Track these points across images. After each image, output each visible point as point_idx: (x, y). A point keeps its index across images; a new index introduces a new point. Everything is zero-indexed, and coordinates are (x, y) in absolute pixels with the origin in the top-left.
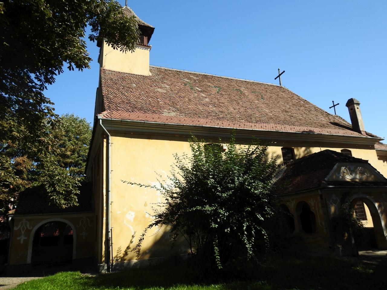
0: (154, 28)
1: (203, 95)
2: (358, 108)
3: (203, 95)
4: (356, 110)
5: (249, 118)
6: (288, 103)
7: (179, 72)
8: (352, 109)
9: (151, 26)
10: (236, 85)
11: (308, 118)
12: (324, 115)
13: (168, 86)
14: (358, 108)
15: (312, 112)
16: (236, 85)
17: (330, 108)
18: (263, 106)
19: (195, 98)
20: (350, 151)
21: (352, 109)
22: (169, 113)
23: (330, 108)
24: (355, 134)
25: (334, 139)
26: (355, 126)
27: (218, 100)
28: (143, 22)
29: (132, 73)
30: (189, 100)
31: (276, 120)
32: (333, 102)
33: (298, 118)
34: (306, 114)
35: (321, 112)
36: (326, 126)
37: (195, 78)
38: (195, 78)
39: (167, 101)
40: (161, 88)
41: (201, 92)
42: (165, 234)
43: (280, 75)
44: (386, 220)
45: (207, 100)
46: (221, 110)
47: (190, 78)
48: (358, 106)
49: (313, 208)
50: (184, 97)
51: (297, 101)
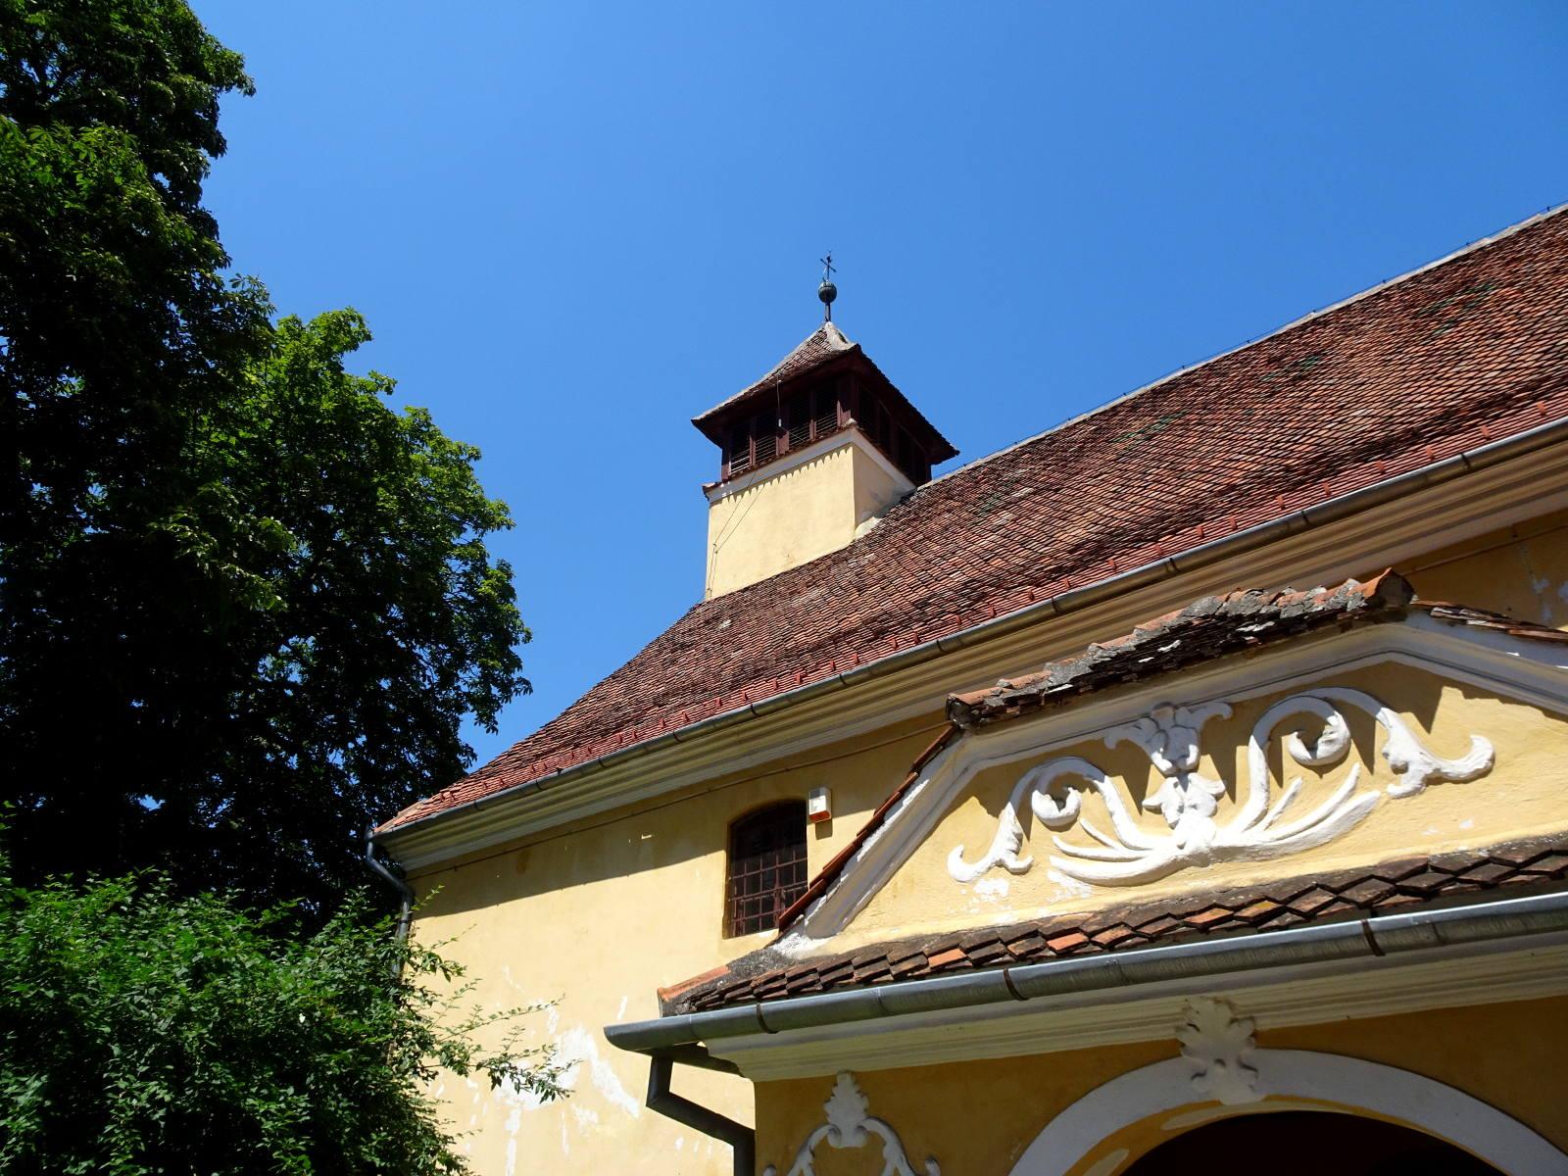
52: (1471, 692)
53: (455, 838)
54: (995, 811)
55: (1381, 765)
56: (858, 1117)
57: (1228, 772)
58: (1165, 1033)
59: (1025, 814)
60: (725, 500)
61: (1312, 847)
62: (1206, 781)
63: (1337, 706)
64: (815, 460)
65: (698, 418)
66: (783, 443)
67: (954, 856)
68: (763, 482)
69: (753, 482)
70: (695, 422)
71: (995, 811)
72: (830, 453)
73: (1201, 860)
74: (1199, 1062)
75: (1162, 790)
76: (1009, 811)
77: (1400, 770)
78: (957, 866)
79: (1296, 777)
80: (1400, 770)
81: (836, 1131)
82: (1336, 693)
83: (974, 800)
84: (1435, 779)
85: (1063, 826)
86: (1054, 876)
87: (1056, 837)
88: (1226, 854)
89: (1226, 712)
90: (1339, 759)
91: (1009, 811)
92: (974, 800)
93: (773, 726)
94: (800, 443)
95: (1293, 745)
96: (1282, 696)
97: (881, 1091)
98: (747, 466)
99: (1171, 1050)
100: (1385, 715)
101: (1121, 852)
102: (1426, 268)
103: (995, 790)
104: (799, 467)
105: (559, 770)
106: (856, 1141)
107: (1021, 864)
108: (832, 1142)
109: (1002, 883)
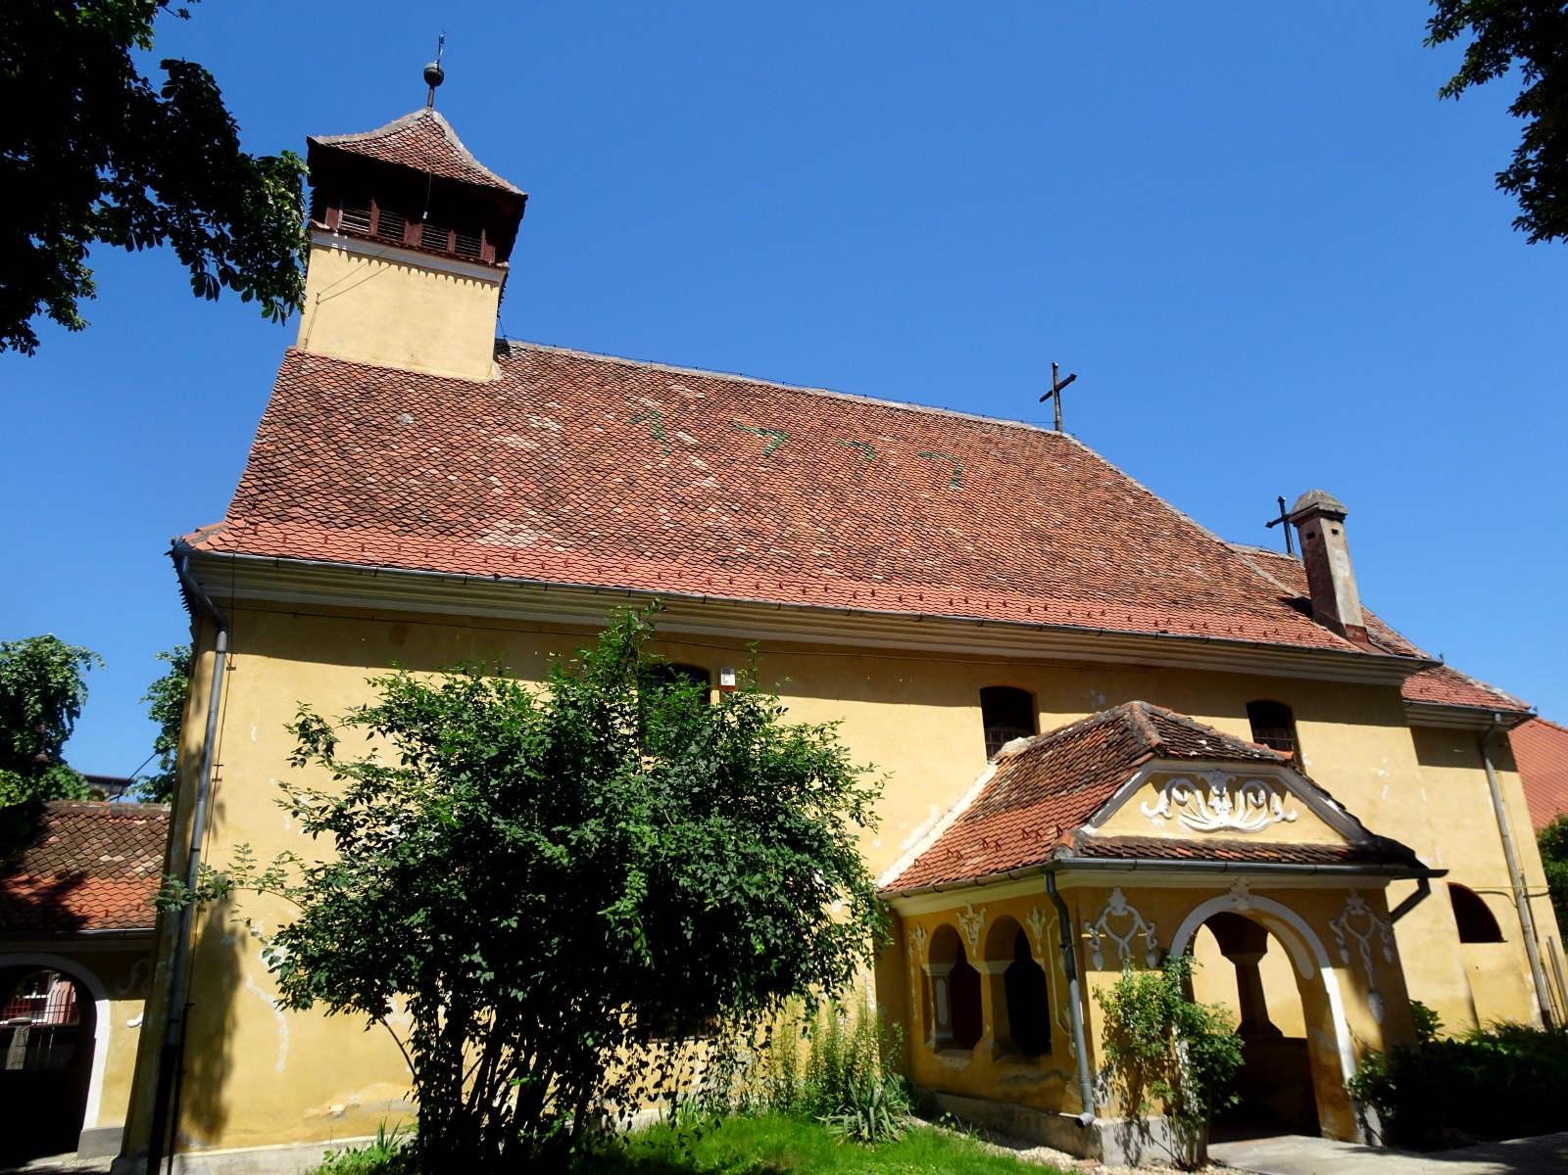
0: (525, 197)
1: (698, 463)
2: (1335, 532)
3: (698, 463)
4: (1328, 537)
5: (859, 563)
6: (1060, 504)
7: (631, 368)
8: (1311, 536)
9: (516, 190)
10: (858, 427)
11: (1133, 565)
12: (1209, 556)
13: (554, 426)
14: (1335, 532)
15: (1160, 543)
16: (858, 427)
17: (1270, 525)
18: (949, 512)
19: (657, 474)
20: (815, 769)
21: (1311, 536)
22: (513, 532)
23: (1270, 525)
24: (1318, 636)
25: (1217, 655)
26: (1318, 602)
27: (756, 483)
28: (485, 171)
29: (418, 370)
30: (631, 483)
31: (981, 572)
32: (1281, 501)
33: (1084, 564)
34: (1130, 550)
35: (1200, 543)
36: (1200, 603)
37: (689, 394)
38: (689, 394)
39: (527, 487)
40: (525, 431)
41: (695, 449)
42: (1012, 965)
43: (1057, 389)
44: (178, 1134)
45: (709, 483)
46: (752, 524)
47: (667, 396)
48: (1337, 526)
49: (1039, 948)
50: (609, 471)
51: (1107, 496)
52: (1294, 795)
53: (302, 585)
54: (1159, 791)
55: (1272, 811)
56: (1124, 905)
57: (1233, 800)
58: (1226, 886)
59: (1169, 795)
60: (334, 252)
61: (1254, 832)
62: (1227, 802)
63: (1263, 788)
64: (457, 276)
65: (321, 140)
66: (414, 234)
67: (1144, 805)
68: (391, 262)
69: (383, 255)
70: (310, 142)
71: (1159, 791)
72: (475, 280)
73: (1226, 829)
74: (1235, 896)
75: (1214, 801)
76: (1164, 793)
77: (1276, 814)
78: (1144, 808)
79: (1252, 809)
80: (1276, 814)
81: (1114, 909)
82: (1264, 784)
83: (1150, 785)
84: (1284, 819)
85: (1183, 804)
86: (1180, 823)
87: (1180, 808)
88: (1233, 829)
89: (1234, 779)
90: (1262, 805)
91: (1164, 793)
92: (1150, 785)
93: (697, 611)
94: (432, 247)
95: (1251, 796)
96: (1254, 779)
97: (1132, 895)
98: (364, 230)
99: (1226, 891)
100: (1274, 795)
101: (1200, 819)
102: (832, 394)
103: (1160, 782)
104: (436, 272)
105: (497, 576)
106: (1125, 913)
107: (1169, 815)
108: (1114, 913)
109: (1161, 821)
